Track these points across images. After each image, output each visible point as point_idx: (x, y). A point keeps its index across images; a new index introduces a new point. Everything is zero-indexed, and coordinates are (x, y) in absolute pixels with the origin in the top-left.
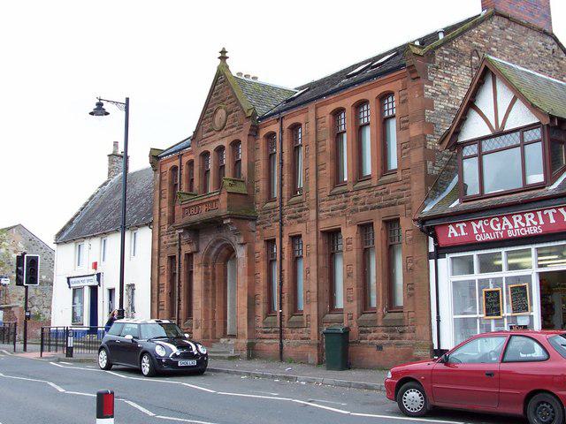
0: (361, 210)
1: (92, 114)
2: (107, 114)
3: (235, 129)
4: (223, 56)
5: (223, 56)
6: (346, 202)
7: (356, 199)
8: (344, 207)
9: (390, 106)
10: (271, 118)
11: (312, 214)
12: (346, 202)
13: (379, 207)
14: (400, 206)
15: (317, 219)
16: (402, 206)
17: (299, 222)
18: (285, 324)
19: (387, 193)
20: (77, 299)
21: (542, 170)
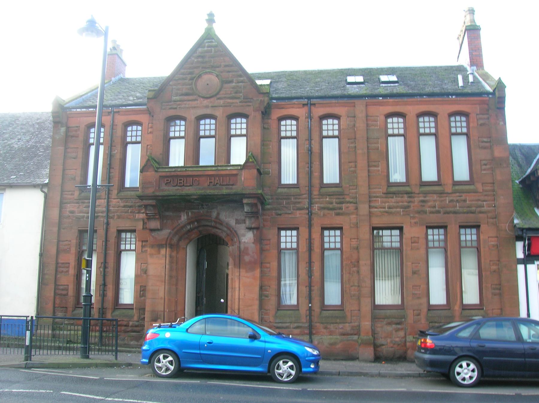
0: (431, 212)
1: (500, 78)
2: (500, 78)
3: (238, 101)
4: (211, 20)
5: (211, 20)
6: (409, 202)
7: (423, 201)
8: (409, 207)
9: (134, 133)
10: (295, 101)
11: (364, 209)
12: (409, 202)
13: (455, 213)
14: (481, 215)
15: (370, 214)
16: (485, 215)
17: (338, 214)
18: (315, 319)
19: (465, 201)
20: (251, 213)
21: (148, 358)
